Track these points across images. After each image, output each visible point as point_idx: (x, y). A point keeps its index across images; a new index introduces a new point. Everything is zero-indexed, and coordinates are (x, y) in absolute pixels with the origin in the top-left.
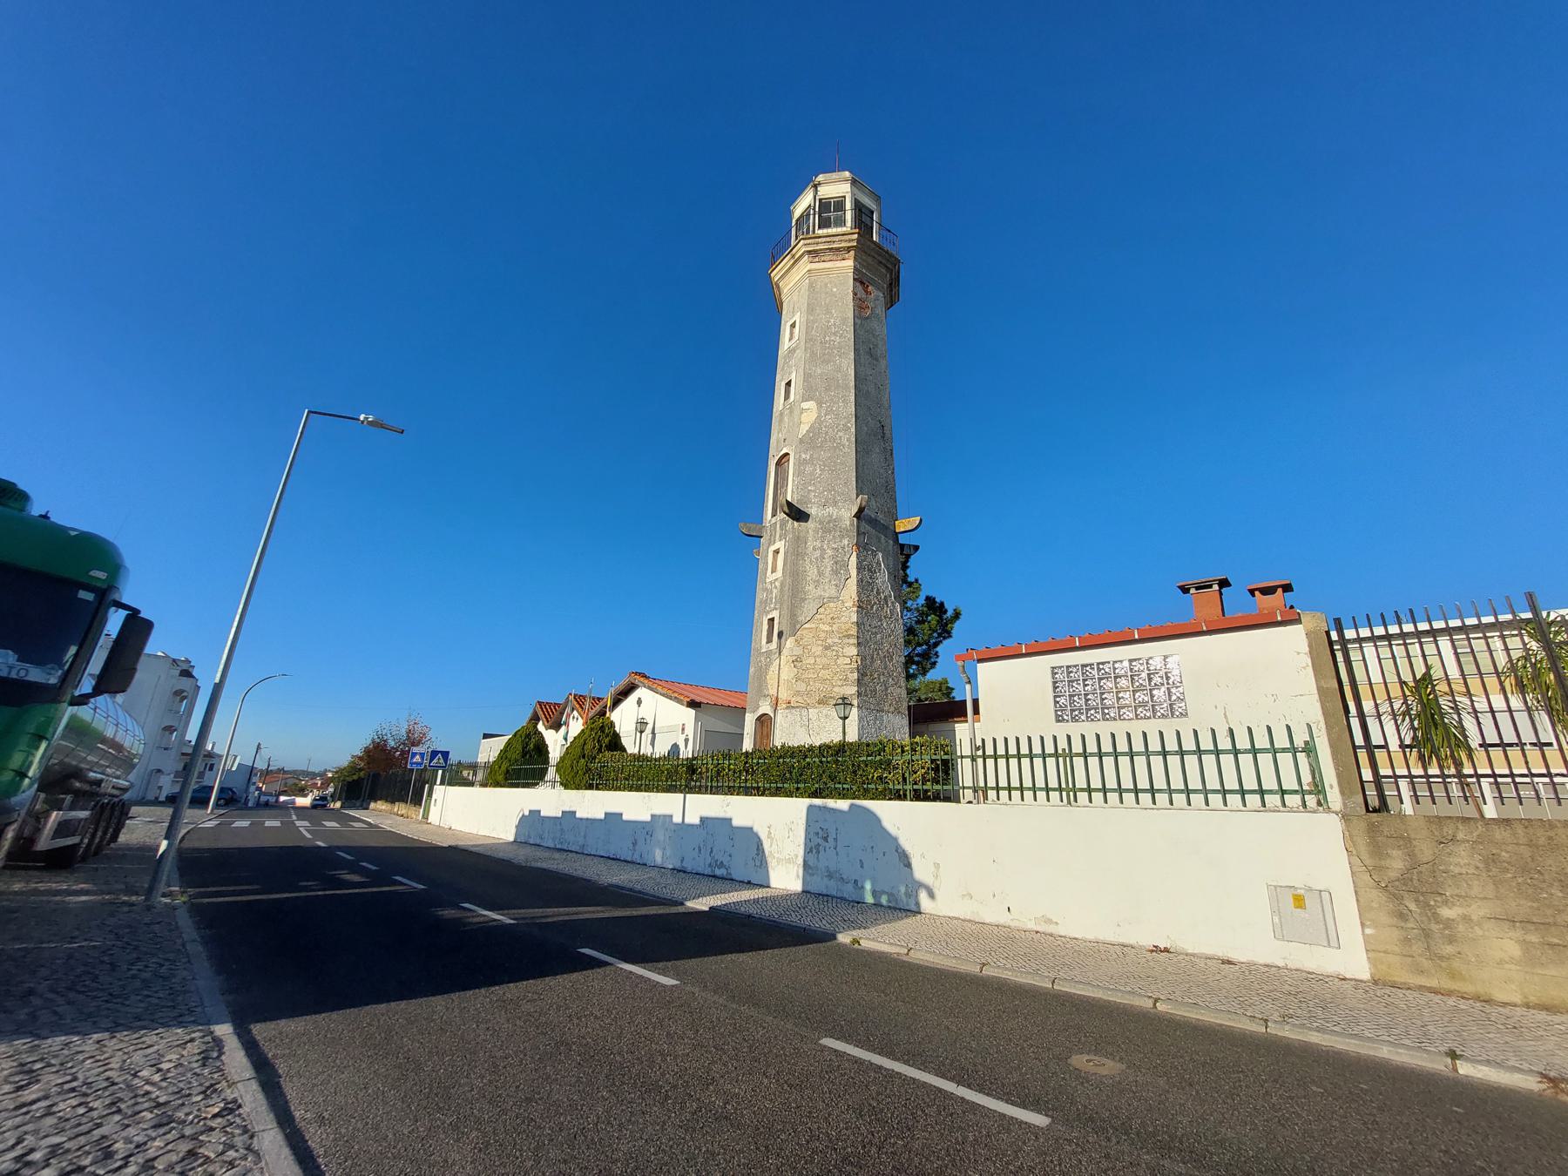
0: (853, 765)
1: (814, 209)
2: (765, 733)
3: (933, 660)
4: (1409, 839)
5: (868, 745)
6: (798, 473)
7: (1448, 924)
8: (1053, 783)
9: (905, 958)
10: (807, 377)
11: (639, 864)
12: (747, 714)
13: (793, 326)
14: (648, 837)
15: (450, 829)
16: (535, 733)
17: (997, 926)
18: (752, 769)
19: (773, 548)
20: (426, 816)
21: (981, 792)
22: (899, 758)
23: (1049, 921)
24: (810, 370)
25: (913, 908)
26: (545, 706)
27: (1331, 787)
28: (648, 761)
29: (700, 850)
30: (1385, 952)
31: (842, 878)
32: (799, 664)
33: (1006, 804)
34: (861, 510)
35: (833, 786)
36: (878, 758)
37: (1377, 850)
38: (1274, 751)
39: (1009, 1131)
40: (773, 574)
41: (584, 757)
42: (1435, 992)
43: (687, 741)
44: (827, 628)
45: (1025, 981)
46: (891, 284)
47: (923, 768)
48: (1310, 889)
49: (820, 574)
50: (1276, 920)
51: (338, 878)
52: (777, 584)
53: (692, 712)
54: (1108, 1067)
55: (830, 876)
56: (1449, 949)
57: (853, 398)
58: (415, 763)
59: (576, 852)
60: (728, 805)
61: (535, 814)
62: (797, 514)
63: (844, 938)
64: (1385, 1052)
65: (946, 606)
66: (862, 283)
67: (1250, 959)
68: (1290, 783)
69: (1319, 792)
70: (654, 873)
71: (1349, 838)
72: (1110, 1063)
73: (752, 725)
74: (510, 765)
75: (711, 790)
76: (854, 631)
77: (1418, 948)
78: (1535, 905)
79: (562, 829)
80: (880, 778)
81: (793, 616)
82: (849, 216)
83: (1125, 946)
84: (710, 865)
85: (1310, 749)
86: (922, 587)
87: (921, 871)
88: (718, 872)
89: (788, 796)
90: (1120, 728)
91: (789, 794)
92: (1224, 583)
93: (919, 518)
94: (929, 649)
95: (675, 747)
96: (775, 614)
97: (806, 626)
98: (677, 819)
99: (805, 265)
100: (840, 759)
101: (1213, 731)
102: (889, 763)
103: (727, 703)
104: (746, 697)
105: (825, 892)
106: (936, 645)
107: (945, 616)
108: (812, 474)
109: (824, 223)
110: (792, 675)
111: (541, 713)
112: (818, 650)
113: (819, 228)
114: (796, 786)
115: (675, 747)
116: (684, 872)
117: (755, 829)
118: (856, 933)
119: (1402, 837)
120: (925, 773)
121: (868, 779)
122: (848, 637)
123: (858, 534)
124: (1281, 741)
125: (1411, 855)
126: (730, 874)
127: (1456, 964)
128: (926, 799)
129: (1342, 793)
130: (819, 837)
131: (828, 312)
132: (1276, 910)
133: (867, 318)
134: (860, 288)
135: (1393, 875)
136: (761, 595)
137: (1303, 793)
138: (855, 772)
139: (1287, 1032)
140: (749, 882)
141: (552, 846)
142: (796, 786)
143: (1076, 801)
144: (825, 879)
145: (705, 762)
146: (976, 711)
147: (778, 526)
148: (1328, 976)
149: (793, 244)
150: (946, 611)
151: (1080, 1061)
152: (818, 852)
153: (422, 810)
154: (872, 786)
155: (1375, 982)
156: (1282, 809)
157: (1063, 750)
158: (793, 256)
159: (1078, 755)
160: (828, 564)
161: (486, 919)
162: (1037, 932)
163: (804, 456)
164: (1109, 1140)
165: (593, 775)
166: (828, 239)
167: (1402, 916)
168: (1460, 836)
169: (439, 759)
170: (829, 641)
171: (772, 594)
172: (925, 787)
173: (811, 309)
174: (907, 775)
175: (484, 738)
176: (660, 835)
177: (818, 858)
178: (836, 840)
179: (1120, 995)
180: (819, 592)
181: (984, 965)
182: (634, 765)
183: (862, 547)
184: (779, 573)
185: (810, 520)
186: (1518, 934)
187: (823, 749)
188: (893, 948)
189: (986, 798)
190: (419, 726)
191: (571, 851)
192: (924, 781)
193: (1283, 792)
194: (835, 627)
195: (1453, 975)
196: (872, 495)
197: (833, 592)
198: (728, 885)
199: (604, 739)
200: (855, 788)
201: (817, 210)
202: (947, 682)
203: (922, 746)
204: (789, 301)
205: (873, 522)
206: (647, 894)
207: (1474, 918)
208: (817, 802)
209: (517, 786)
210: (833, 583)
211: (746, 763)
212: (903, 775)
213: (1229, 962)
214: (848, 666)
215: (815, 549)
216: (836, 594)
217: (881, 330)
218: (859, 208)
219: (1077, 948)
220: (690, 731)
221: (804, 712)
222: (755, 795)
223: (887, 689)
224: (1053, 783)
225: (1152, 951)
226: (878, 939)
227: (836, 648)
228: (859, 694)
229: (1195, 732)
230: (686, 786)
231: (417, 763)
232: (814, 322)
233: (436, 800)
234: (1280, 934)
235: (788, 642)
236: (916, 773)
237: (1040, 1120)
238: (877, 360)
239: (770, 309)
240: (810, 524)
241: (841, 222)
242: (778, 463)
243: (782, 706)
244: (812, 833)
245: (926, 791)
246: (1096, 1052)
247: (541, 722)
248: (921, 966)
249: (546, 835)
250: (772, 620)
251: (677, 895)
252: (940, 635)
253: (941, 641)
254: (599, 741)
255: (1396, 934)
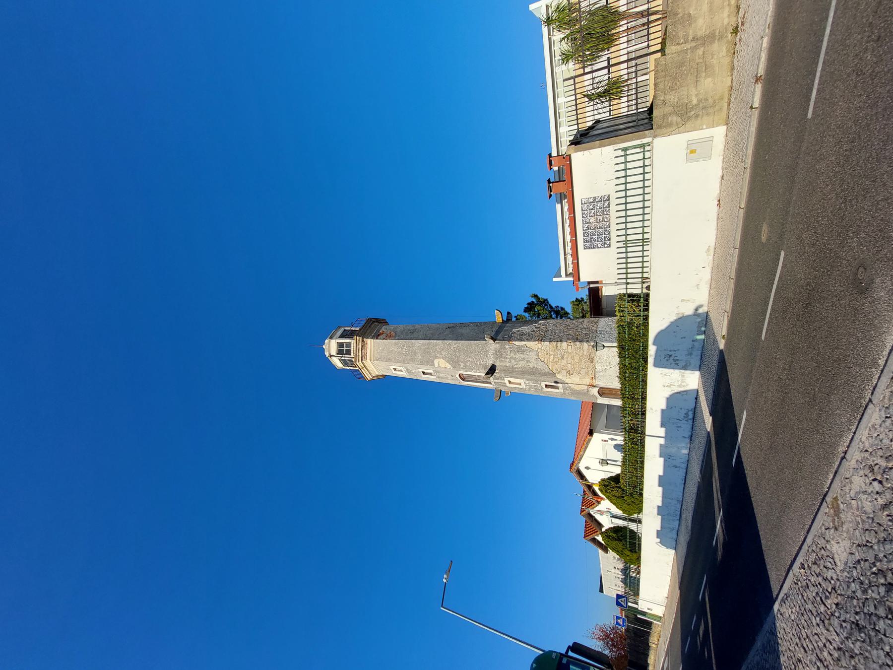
0: (630, 341)
1: (341, 357)
2: (609, 392)
3: (560, 309)
4: (664, 115)
5: (619, 333)
6: (470, 369)
7: (699, 101)
8: (640, 248)
9: (730, 313)
10: (422, 363)
11: (688, 464)
12: (598, 402)
13: (395, 369)
14: (672, 458)
15: (667, 598)
16: (607, 533)
17: (712, 273)
18: (631, 395)
19: (508, 384)
20: (659, 618)
21: (644, 280)
22: (627, 318)
23: (708, 250)
24: (418, 362)
25: (705, 315)
26: (587, 534)
27: (641, 141)
28: (626, 456)
29: (678, 427)
30: (713, 121)
31: (692, 348)
32: (571, 372)
33: (650, 269)
34: (492, 338)
35: (641, 352)
36: (626, 328)
37: (670, 125)
38: (626, 162)
39: (786, 265)
40: (520, 384)
41: (623, 497)
42: (729, 104)
43: (612, 439)
44: (552, 357)
45: (736, 260)
46: (379, 322)
47: (632, 307)
48: (687, 148)
49: (523, 359)
50: (701, 160)
51: (702, 641)
52: (527, 382)
53: (595, 435)
54: (765, 229)
55: (691, 354)
56: (710, 100)
57: (435, 341)
58: (623, 623)
59: (682, 505)
60: (652, 409)
61: (659, 534)
62: (492, 370)
63: (722, 347)
64: (753, 129)
65: (529, 301)
66: (379, 335)
67: (720, 168)
68: (641, 156)
69: (644, 146)
70: (693, 454)
71: (663, 135)
72: (764, 228)
73: (604, 399)
74: (627, 549)
75: (643, 419)
76: (554, 344)
77: (711, 110)
78: (690, 75)
79: (667, 514)
80: (637, 328)
81: (545, 374)
82: (348, 341)
83: (718, 218)
84: (687, 421)
85: (625, 150)
86: (519, 314)
87: (689, 310)
88: (691, 416)
89: (647, 376)
90: (614, 221)
91: (646, 375)
92: (549, 182)
93: (496, 311)
94: (554, 311)
95: (616, 447)
96: (543, 384)
97: (550, 368)
98: (662, 441)
99: (368, 362)
100: (627, 348)
101: (616, 185)
102: (629, 323)
103: (590, 415)
104: (586, 402)
105: (700, 357)
106: (551, 307)
107: (536, 302)
108: (471, 362)
109: (348, 352)
110: (577, 376)
111: (589, 536)
112: (564, 362)
113: (350, 355)
114: (641, 371)
115: (616, 447)
116: (691, 436)
117: (667, 396)
118: (719, 338)
119: (663, 117)
120: (635, 306)
121: (638, 334)
122: (557, 346)
123: (504, 340)
124: (622, 159)
125: (671, 114)
126: (692, 409)
127: (716, 98)
128: (648, 305)
129: (645, 138)
130: (668, 360)
131: (391, 352)
132: (698, 160)
133: (396, 334)
134: (381, 337)
135: (679, 119)
136: (532, 392)
137: (644, 152)
138: (634, 340)
139: (749, 161)
140: (696, 398)
141: (678, 522)
142: (641, 371)
143: (648, 239)
144: (693, 356)
145: (627, 422)
146: (597, 282)
147: (496, 381)
148: (726, 140)
149: (357, 368)
150: (533, 302)
151: (764, 238)
152: (678, 360)
153: (655, 622)
154: (641, 331)
155: (727, 124)
156: (651, 159)
157: (624, 244)
158: (363, 368)
159: (626, 238)
160: (518, 355)
161: (721, 530)
162: (714, 255)
163: (462, 366)
164: (786, 231)
165: (634, 492)
166: (357, 350)
167: (697, 116)
168: (662, 99)
169: (621, 601)
170: (559, 356)
171: (532, 385)
172: (642, 306)
173: (389, 360)
174: (636, 315)
175: (603, 592)
176: (673, 450)
177: (681, 360)
178: (670, 351)
179: (739, 222)
180: (533, 360)
181: (730, 278)
182: (628, 465)
183: (510, 339)
184: (522, 381)
185: (495, 364)
186: (702, 80)
187: (621, 356)
188: (725, 319)
189: (647, 278)
190: (595, 631)
191: (681, 508)
192: (639, 306)
193: (644, 158)
194: (552, 353)
195: (721, 98)
196: (484, 333)
197: (533, 354)
198: (698, 410)
199: (611, 485)
200: (642, 341)
201: (342, 356)
202: (573, 302)
203: (621, 307)
204: (382, 371)
205: (498, 332)
206: (705, 450)
207: (696, 93)
208: (651, 360)
209: (640, 545)
210: (528, 353)
211: (628, 398)
212: (635, 316)
213: (723, 177)
214: (573, 346)
215: (510, 362)
216: (535, 352)
217: (401, 327)
218: (343, 336)
219: (720, 238)
220: (606, 437)
221: (597, 370)
222: (646, 394)
223: (585, 328)
224: (640, 248)
225: (720, 207)
226: (721, 327)
227: (563, 353)
228: (588, 341)
229: (616, 192)
230: (641, 434)
231: (623, 622)
232: (395, 359)
233: (648, 609)
234: (709, 157)
235: (559, 377)
236: (634, 310)
237: (783, 253)
238: (416, 329)
239: (384, 379)
240: (497, 364)
241: (349, 345)
242: (463, 380)
243: (594, 383)
244: (667, 363)
245: (644, 306)
246: (760, 232)
247: (596, 537)
248: (733, 305)
249: (671, 526)
250: (546, 386)
251: (705, 435)
252: (546, 305)
253: (550, 305)
254: (613, 488)
255: (705, 118)
